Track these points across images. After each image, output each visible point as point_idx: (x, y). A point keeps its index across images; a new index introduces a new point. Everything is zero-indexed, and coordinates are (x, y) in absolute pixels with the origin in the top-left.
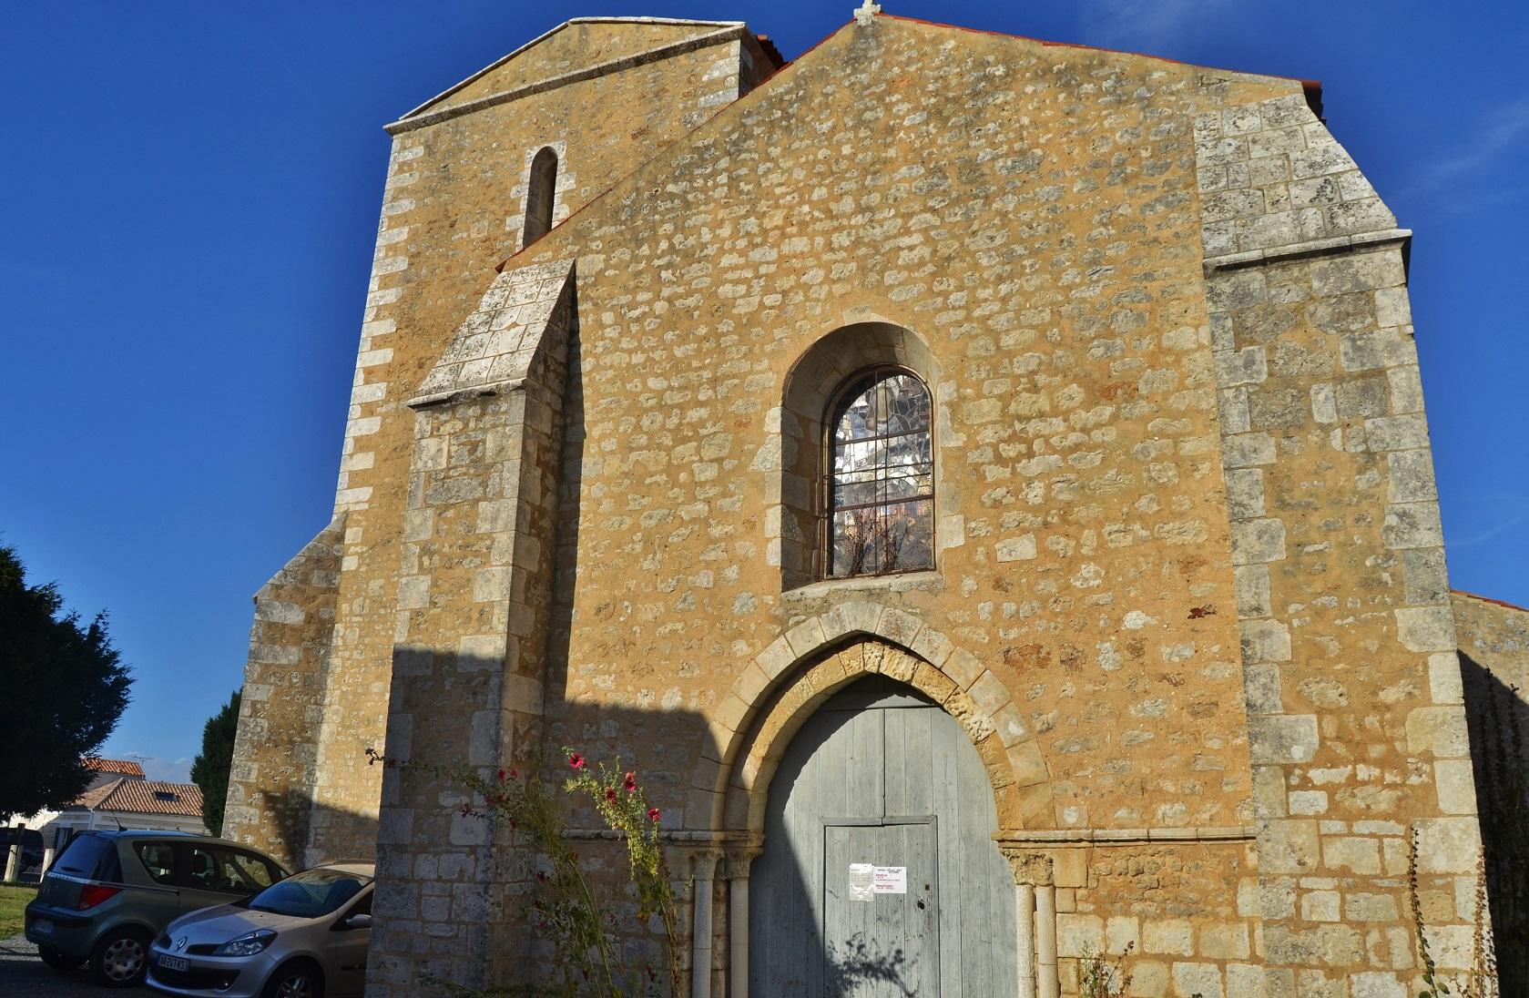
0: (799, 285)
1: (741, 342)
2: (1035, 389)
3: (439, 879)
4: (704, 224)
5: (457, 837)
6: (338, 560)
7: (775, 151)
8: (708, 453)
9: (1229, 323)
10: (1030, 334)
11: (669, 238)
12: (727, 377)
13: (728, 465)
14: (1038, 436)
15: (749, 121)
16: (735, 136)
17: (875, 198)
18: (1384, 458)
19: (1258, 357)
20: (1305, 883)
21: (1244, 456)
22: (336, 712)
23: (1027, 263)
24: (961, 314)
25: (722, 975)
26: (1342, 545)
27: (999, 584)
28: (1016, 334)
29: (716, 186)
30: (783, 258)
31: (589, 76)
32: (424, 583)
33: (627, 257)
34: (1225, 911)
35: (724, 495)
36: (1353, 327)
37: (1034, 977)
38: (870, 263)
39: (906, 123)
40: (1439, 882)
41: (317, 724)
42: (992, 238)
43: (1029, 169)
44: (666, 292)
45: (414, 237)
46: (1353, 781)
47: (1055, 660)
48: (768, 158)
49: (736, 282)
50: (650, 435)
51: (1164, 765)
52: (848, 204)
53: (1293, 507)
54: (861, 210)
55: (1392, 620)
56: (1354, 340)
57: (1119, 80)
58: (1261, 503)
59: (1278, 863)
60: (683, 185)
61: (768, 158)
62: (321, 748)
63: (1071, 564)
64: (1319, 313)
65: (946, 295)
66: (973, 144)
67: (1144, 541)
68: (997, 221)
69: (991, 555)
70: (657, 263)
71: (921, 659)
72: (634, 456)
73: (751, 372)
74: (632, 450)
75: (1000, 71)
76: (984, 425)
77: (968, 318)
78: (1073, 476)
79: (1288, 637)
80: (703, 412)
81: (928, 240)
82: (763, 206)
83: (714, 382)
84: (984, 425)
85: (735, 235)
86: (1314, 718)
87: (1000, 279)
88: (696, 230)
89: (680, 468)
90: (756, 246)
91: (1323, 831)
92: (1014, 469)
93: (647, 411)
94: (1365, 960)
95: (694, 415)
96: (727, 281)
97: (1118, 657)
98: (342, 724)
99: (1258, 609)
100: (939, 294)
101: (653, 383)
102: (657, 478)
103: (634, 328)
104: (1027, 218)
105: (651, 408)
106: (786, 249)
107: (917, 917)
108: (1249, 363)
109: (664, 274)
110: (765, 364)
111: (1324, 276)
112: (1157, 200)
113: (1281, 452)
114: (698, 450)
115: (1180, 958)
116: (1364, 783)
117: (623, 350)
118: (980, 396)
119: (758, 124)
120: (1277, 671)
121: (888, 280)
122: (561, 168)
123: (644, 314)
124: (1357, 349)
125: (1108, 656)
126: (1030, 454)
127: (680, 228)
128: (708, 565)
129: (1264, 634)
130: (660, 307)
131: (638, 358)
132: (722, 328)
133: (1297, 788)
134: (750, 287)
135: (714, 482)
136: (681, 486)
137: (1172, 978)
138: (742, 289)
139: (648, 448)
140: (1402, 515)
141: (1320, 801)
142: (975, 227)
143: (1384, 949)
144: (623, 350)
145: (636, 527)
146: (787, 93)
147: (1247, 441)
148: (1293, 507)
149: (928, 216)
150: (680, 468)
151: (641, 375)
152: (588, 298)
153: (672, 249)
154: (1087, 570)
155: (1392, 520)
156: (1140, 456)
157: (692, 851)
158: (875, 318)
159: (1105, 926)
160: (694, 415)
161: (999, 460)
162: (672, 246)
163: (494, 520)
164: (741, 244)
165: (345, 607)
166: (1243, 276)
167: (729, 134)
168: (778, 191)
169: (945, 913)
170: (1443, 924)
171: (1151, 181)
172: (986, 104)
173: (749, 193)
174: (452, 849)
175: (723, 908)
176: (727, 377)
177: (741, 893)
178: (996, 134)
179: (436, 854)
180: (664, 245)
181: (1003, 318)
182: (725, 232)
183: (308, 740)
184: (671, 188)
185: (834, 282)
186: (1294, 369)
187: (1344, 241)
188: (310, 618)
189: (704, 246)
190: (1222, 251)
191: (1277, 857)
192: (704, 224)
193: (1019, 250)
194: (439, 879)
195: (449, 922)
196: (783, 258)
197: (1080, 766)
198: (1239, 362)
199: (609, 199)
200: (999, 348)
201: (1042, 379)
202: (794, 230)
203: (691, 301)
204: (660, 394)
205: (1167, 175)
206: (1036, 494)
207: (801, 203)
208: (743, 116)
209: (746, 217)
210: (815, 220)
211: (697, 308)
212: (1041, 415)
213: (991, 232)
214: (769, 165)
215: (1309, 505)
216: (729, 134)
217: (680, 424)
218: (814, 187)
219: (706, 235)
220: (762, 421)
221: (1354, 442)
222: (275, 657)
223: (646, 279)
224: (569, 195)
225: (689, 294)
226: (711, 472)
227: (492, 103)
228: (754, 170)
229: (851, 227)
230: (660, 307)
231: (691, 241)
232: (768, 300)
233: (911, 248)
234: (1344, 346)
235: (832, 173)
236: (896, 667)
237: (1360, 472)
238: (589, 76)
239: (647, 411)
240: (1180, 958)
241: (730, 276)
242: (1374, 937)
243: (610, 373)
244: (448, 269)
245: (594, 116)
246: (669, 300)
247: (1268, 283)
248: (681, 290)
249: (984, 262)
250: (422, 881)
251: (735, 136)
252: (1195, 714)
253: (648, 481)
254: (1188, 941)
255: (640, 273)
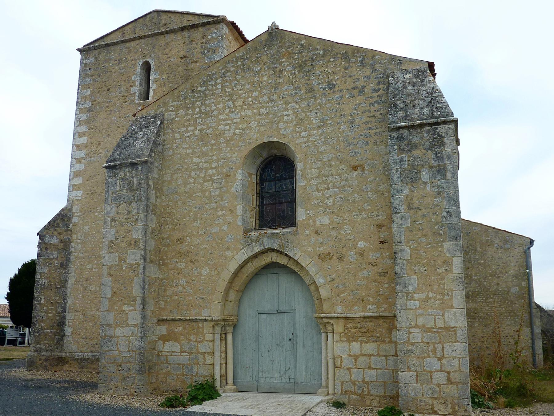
0: (248, 127)
1: (227, 146)
2: (330, 166)
3: (124, 336)
4: (213, 103)
5: (130, 321)
6: (70, 219)
7: (239, 77)
8: (215, 186)
9: (396, 147)
10: (330, 147)
11: (199, 107)
12: (222, 159)
13: (223, 190)
14: (331, 182)
15: (228, 65)
16: (223, 71)
17: (276, 97)
18: (443, 194)
19: (405, 159)
20: (411, 330)
21: (398, 192)
22: (74, 276)
23: (329, 122)
24: (305, 139)
25: (224, 365)
26: (428, 221)
27: (317, 232)
28: (324, 147)
29: (216, 89)
30: (242, 117)
31: (162, 33)
32: (113, 231)
33: (184, 114)
34: (387, 340)
35: (222, 200)
36: (436, 150)
37: (327, 363)
38: (274, 120)
39: (287, 70)
40: (452, 329)
41: (66, 280)
42: (317, 113)
43: (331, 88)
44: (199, 128)
45: (93, 93)
46: (427, 298)
47: (335, 257)
48: (236, 80)
49: (225, 125)
50: (195, 179)
51: (369, 292)
52: (266, 98)
53: (413, 209)
54: (271, 101)
55: (442, 246)
56: (436, 154)
57: (364, 58)
58: (403, 207)
59: (403, 324)
60: (204, 88)
61: (236, 80)
62: (68, 289)
63: (341, 225)
64: (426, 144)
65: (300, 132)
66: (311, 78)
67: (365, 218)
68: (319, 107)
69: (314, 222)
70: (195, 116)
71: (291, 257)
72: (189, 186)
73: (231, 157)
74: (188, 184)
75: (321, 52)
76: (313, 178)
77: (308, 141)
78: (341, 196)
79: (409, 251)
80: (214, 171)
81: (294, 113)
82: (235, 97)
83: (218, 160)
84: (313, 178)
85: (224, 107)
86: (416, 277)
87: (319, 127)
88: (209, 105)
89: (206, 191)
90: (232, 112)
91: (417, 314)
92: (323, 193)
93: (193, 170)
94: (429, 355)
95: (210, 172)
96: (221, 124)
97: (355, 256)
98: (76, 281)
99: (400, 242)
100: (298, 132)
101: (195, 160)
102: (198, 194)
103: (188, 140)
104: (329, 107)
105: (195, 169)
106: (243, 114)
107: (289, 345)
108: (402, 160)
109: (198, 121)
110: (236, 155)
111: (428, 132)
112: (375, 102)
113: (411, 191)
114: (212, 184)
115: (373, 355)
116: (431, 298)
117: (183, 148)
118: (312, 168)
119: (232, 67)
120: (405, 262)
121: (280, 127)
122: (152, 70)
123: (191, 135)
124: (437, 157)
125: (352, 256)
126: (328, 189)
127: (203, 104)
128: (217, 225)
129: (402, 250)
130: (197, 132)
131: (189, 151)
132: (220, 141)
133: (410, 300)
134: (230, 127)
135: (218, 196)
136: (206, 197)
137: (370, 362)
138: (227, 127)
139: (194, 183)
140: (448, 212)
141: (417, 304)
142: (311, 109)
143: (434, 351)
144: (183, 148)
145: (190, 211)
146: (243, 56)
147: (399, 187)
148: (413, 209)
149: (294, 104)
150: (206, 191)
151: (191, 157)
152: (169, 128)
153: (201, 112)
154: (346, 227)
155: (445, 214)
156: (365, 190)
157: (212, 324)
158: (275, 140)
159: (350, 345)
160: (210, 172)
161: (318, 190)
162: (200, 110)
163: (138, 209)
164: (227, 111)
165: (74, 237)
166: (401, 132)
167: (221, 70)
168: (240, 92)
169: (298, 342)
170: (453, 342)
171: (373, 95)
172: (316, 64)
173: (229, 92)
174: (128, 325)
175: (224, 342)
176: (222, 159)
177: (230, 337)
178: (320, 75)
179: (122, 327)
180: (198, 110)
181: (320, 142)
182: (221, 106)
183: (63, 287)
184: (199, 88)
185: (261, 126)
186: (416, 163)
187: (435, 120)
188: (61, 241)
189: (213, 111)
190: (395, 122)
191: (403, 322)
192: (213, 103)
193: (326, 118)
194: (124, 336)
195: (129, 351)
196: (242, 117)
197: (343, 292)
198: (398, 161)
199: (176, 91)
200: (318, 152)
201: (332, 163)
202: (246, 107)
203: (208, 131)
204: (198, 164)
205: (379, 93)
206: (329, 202)
207: (248, 97)
208: (226, 63)
209: (228, 101)
210: (253, 104)
211: (211, 134)
212: (332, 175)
213: (317, 111)
214: (237, 82)
215: (418, 208)
216: (221, 70)
217: (206, 175)
218: (253, 91)
219: (214, 108)
220: (235, 175)
221: (434, 188)
222: (48, 256)
223: (192, 123)
224: (156, 80)
225: (208, 128)
226: (217, 192)
227: (123, 42)
228: (231, 84)
229: (267, 107)
230: (197, 132)
231: (208, 109)
232: (237, 132)
233: (288, 115)
234: (433, 156)
235: (260, 87)
236: (282, 260)
237: (435, 198)
238: (162, 33)
239: (193, 170)
240: (373, 355)
241: (223, 122)
242: (431, 347)
243: (179, 156)
244: (108, 107)
245: (165, 49)
246: (200, 131)
247: (410, 134)
248: (205, 127)
249: (314, 121)
250: (118, 337)
251: (223, 71)
252: (380, 276)
253: (194, 195)
254: (376, 350)
255: (188, 120)
